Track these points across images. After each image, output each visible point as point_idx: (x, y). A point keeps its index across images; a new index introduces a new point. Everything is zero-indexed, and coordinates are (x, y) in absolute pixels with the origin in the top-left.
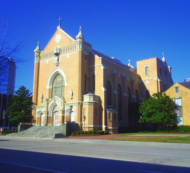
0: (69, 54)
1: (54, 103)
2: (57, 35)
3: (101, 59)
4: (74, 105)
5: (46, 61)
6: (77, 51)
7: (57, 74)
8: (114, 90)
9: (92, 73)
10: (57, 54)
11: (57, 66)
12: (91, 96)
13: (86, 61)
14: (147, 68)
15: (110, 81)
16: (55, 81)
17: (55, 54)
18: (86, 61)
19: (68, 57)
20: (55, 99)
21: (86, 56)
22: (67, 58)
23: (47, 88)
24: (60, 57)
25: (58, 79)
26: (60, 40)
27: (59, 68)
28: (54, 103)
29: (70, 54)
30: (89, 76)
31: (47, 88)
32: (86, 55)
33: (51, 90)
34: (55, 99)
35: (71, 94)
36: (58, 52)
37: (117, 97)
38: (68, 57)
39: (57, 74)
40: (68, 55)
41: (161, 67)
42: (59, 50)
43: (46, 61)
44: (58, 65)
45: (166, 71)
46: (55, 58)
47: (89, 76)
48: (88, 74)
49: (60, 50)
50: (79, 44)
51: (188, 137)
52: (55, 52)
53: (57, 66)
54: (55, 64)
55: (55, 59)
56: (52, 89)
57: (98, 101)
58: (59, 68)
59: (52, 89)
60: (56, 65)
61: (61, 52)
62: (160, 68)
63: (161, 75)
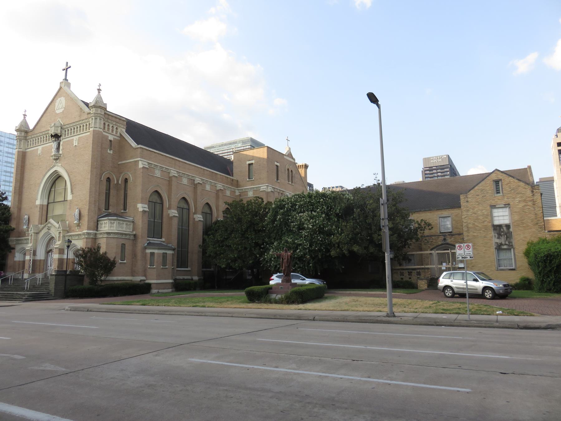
0: (77, 137)
1: (48, 233)
2: (59, 99)
3: (11, 162)
4: (73, 238)
5: (38, 149)
6: (89, 133)
7: (56, 178)
8: (170, 208)
9: (123, 174)
10: (56, 137)
11: (55, 159)
12: (112, 222)
13: (111, 152)
14: (251, 167)
15: (160, 192)
16: (53, 189)
17: (52, 136)
18: (111, 152)
19: (75, 143)
20: (49, 225)
21: (111, 141)
22: (74, 145)
23: (37, 204)
24: (61, 143)
25: (59, 186)
26: (63, 109)
27: (60, 164)
28: (48, 233)
29: (79, 138)
30: (118, 181)
31: (37, 204)
32: (112, 139)
33: (45, 208)
34: (49, 225)
35: (77, 217)
36: (58, 132)
37: (175, 222)
38: (75, 143)
39: (56, 178)
40: (75, 140)
41: (278, 164)
42: (59, 128)
43: (38, 149)
44: (57, 159)
45: (292, 171)
46: (52, 143)
47: (118, 181)
48: (115, 178)
49: (62, 128)
50: (93, 118)
51: (223, 302)
52: (52, 131)
53: (55, 159)
54: (52, 156)
55: (53, 146)
56: (48, 205)
57: (131, 230)
58: (60, 164)
59: (48, 205)
60: (53, 157)
61: (63, 132)
62: (277, 166)
63: (277, 179)
